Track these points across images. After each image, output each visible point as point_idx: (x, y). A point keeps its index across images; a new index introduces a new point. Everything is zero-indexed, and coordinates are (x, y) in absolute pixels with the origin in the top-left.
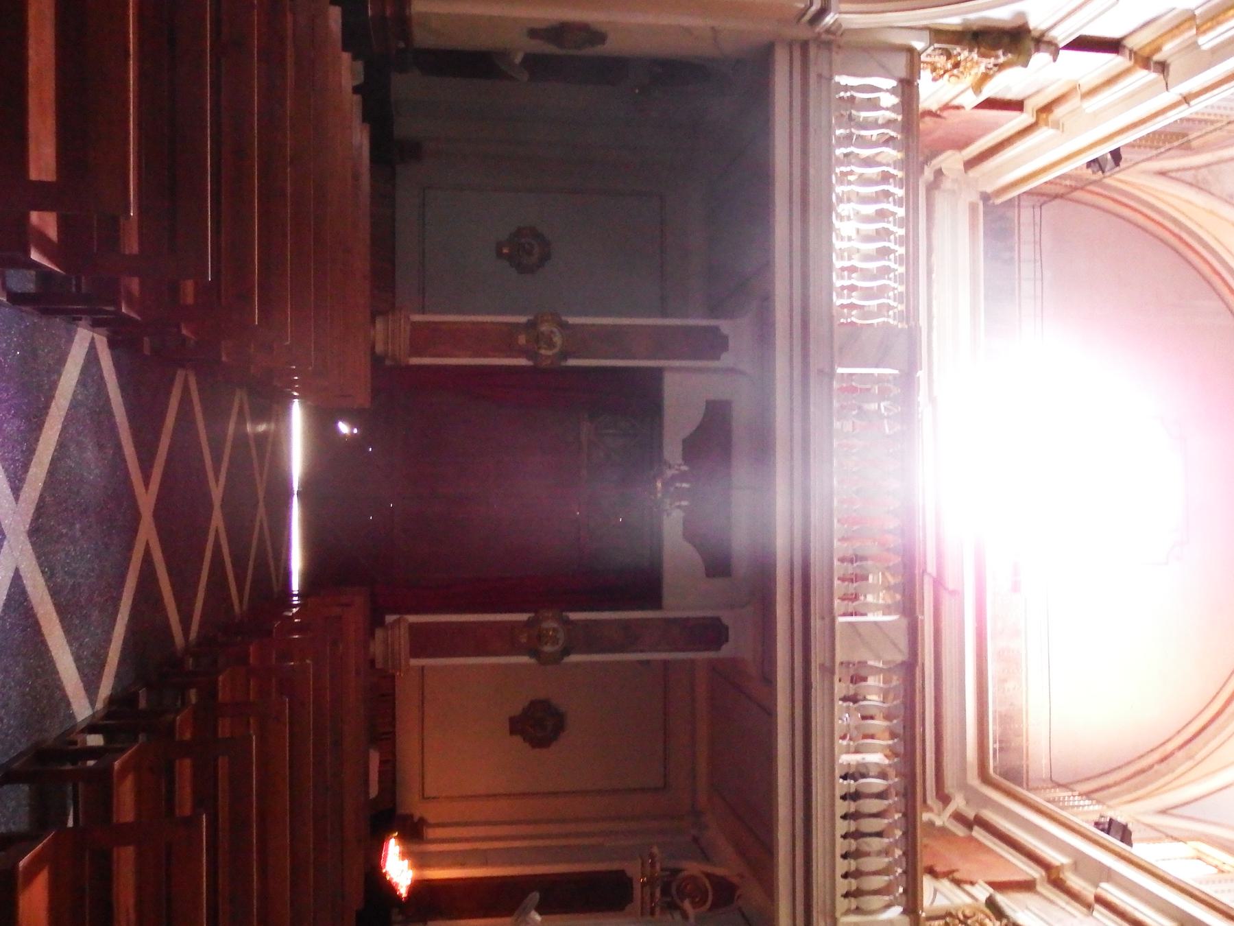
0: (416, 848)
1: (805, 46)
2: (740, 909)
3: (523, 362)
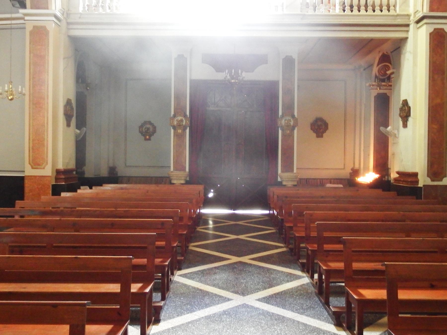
0: (362, 171)
1: (68, 24)
2: (392, 52)
3: (188, 131)
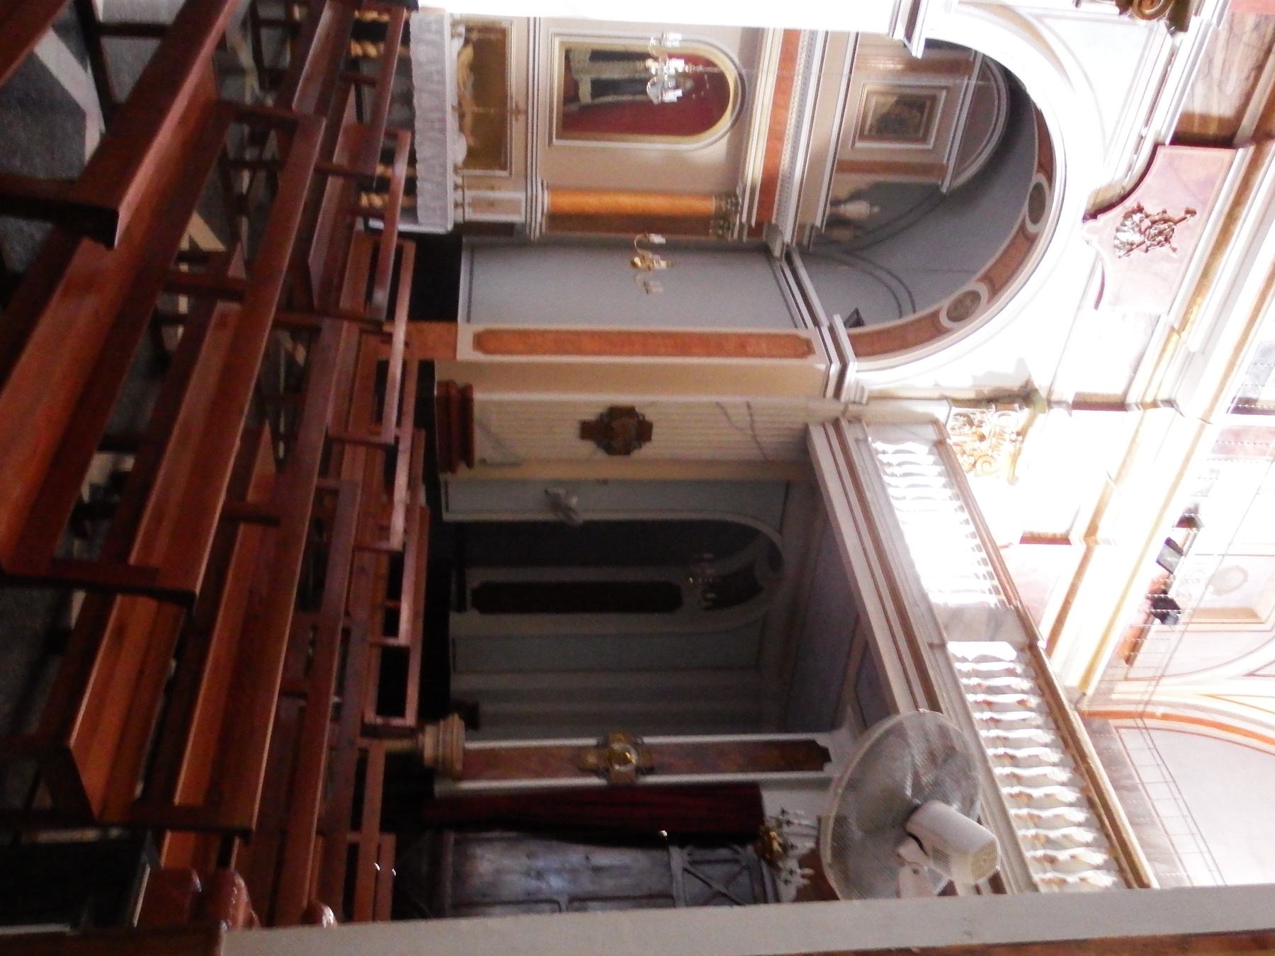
1: (836, 423)
3: (594, 781)
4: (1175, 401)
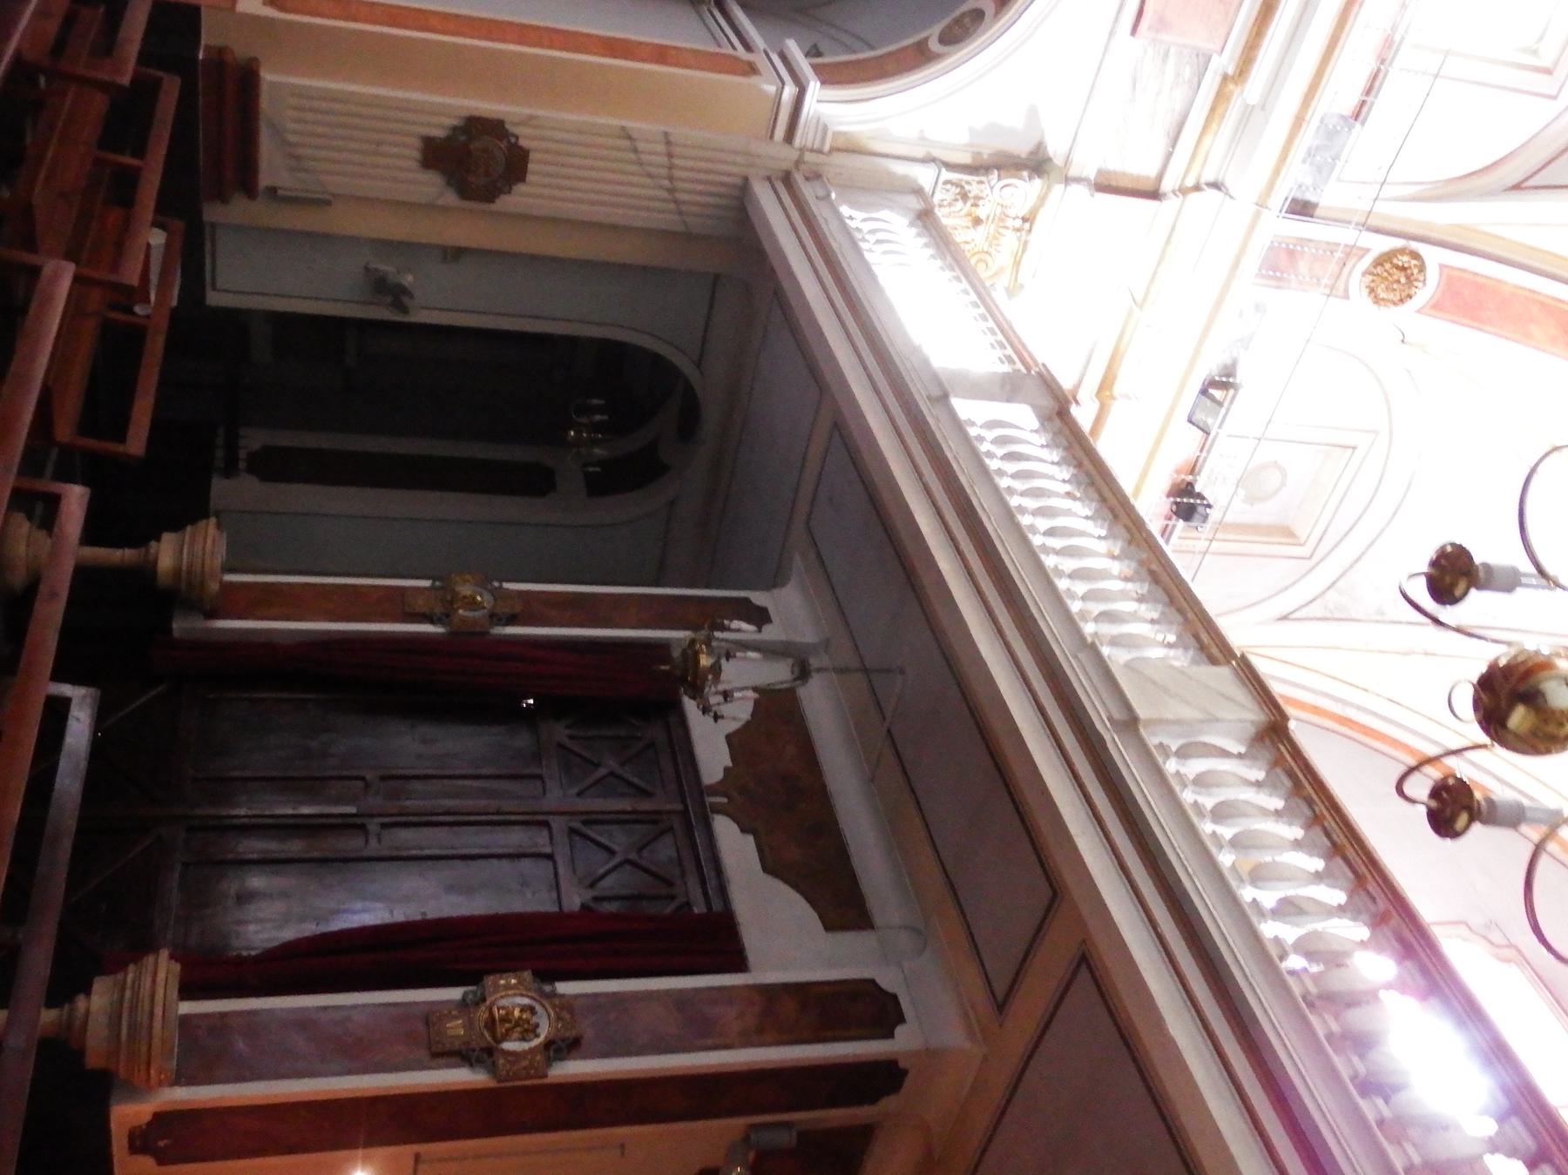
1: (787, 179)
4: (1223, 184)
